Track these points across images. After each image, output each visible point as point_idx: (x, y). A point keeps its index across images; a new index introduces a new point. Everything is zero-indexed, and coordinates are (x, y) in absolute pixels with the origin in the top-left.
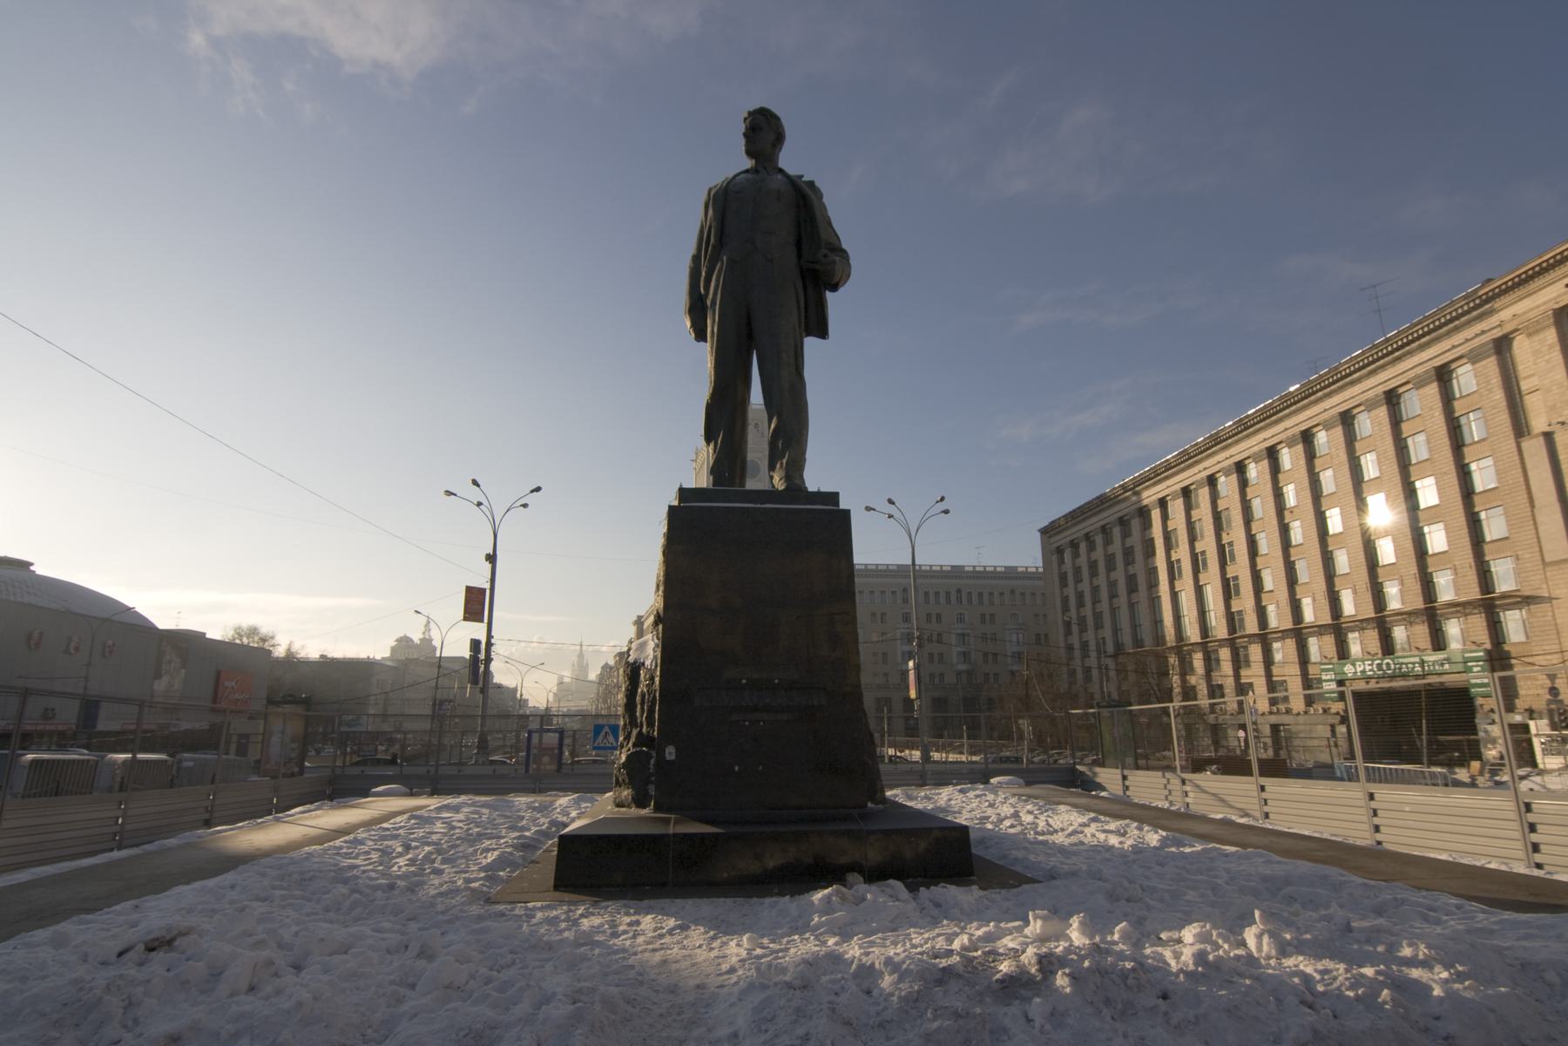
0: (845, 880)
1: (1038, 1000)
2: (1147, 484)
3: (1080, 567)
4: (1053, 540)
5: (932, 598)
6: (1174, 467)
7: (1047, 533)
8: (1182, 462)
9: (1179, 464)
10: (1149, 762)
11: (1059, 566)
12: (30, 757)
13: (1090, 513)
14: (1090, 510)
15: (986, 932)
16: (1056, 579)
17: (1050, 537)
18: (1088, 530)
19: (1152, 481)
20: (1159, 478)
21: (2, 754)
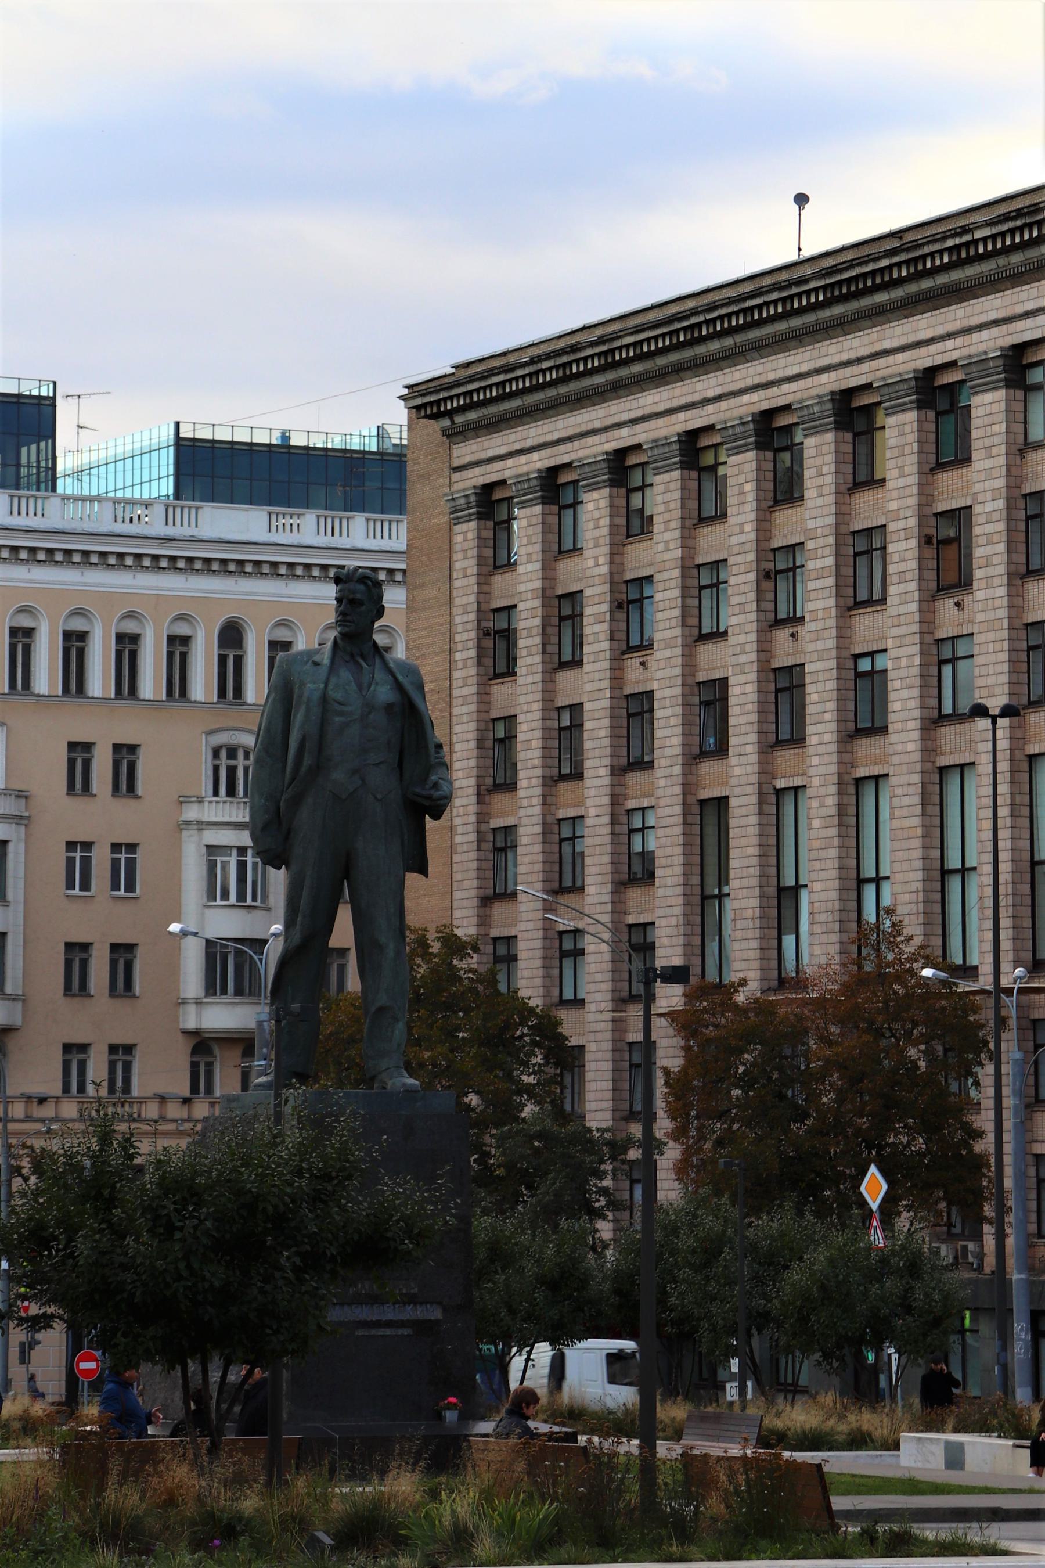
0: (24, 1411)
1: (486, 1427)
2: (881, 297)
3: (574, 597)
4: (466, 451)
5: (97, 1068)
6: (987, 256)
7: (450, 414)
8: (1015, 248)
9: (1006, 251)
10: (894, 918)
11: (483, 581)
12: (968, 1316)
13: (637, 368)
14: (641, 357)
15: (365, 1480)
16: (466, 636)
17: (453, 435)
18: (624, 438)
19: (898, 293)
20: (926, 284)
21: (2, 1459)
